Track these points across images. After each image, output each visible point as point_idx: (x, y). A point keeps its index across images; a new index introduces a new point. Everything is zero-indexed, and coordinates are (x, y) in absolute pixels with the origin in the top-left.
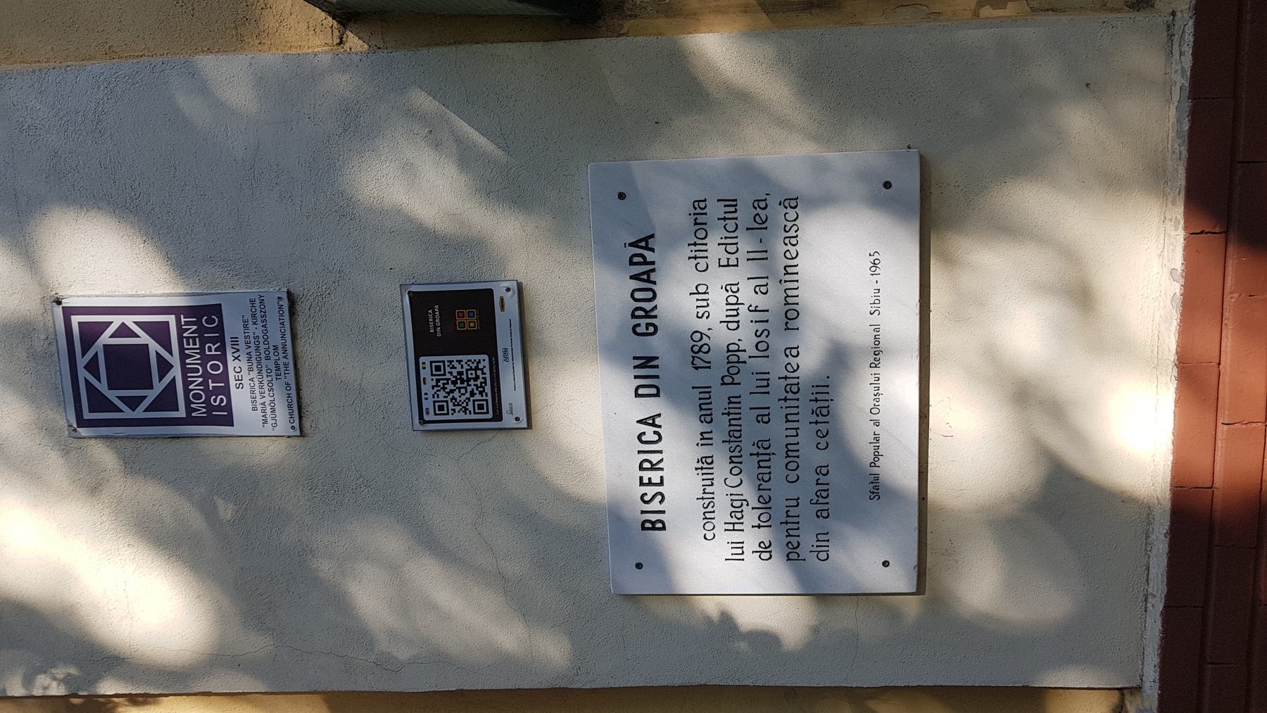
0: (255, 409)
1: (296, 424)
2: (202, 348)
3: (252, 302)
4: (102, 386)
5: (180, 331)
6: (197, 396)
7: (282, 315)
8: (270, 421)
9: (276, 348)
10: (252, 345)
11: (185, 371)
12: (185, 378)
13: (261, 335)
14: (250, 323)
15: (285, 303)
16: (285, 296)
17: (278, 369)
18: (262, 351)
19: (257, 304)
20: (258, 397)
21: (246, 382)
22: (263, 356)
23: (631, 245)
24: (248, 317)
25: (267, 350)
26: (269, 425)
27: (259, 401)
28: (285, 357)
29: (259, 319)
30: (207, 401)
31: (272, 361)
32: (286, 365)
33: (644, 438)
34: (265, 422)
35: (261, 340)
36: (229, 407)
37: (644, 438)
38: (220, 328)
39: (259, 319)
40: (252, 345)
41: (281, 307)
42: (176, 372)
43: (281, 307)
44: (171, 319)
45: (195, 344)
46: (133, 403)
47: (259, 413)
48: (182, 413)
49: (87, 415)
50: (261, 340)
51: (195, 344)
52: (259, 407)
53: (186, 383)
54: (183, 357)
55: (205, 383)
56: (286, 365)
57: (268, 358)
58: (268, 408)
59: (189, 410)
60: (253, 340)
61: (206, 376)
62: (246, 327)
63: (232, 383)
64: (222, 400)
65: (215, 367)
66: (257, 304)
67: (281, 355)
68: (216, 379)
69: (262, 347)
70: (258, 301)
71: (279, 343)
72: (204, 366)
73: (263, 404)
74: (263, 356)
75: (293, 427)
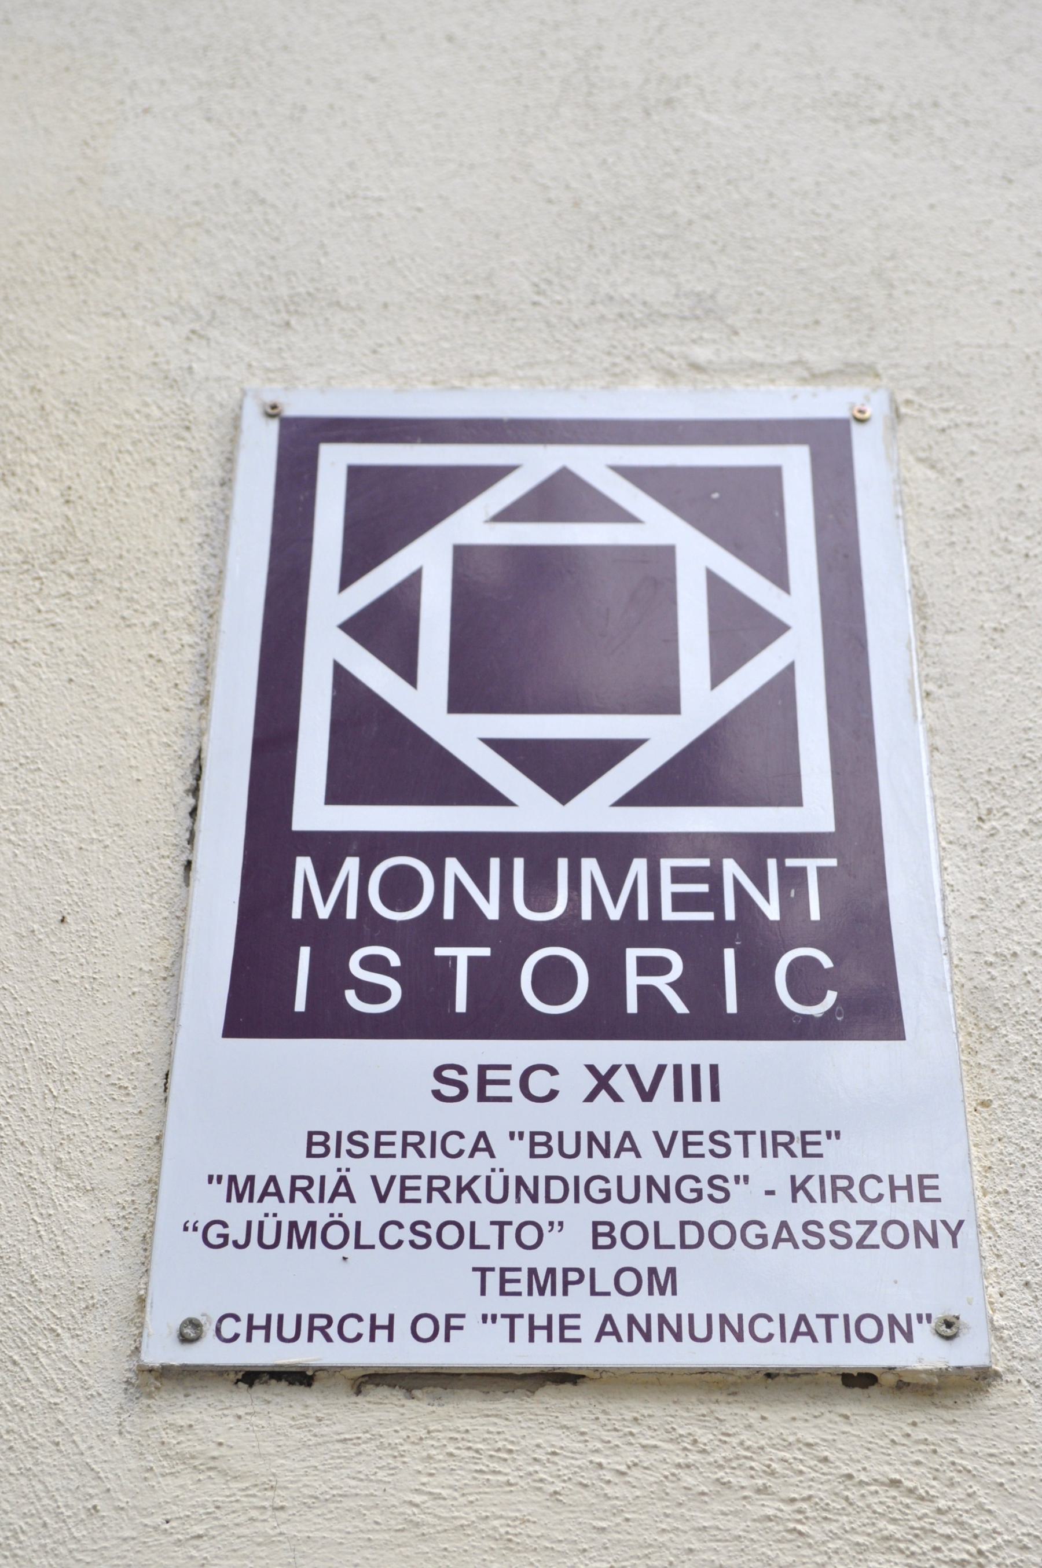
0: (316, 1143)
1: (208, 1352)
2: (656, 931)
3: (922, 1187)
4: (473, 524)
5: (754, 850)
6: (401, 888)
7: (853, 1329)
8: (238, 1215)
9: (664, 1282)
10: (676, 1166)
11: (542, 851)
12: (507, 845)
13: (736, 1211)
14: (802, 1167)
15: (924, 1354)
16: (967, 1353)
17: (542, 1282)
18: (647, 1211)
19: (908, 1211)
20: (384, 1170)
21: (470, 1116)
22: (616, 1213)
23: (343, 1179)
24: (835, 1159)
25: (651, 1236)
26: (213, 1203)
27: (361, 1172)
28: (607, 1328)
29: (826, 1213)
30: (371, 929)
31: (585, 1257)
32: (562, 1328)
33: (241, 1242)
34: (239, 1189)
35: (706, 1213)
36: (329, 1020)
37: (241, 1242)
38: (762, 1021)
39: (826, 1213)
40: (676, 1166)
41: (900, 1328)
42: (531, 809)
43: (900, 1328)
44: (816, 812)
45: (681, 902)
46: (387, 628)
47: (289, 1162)
48: (312, 810)
49: (334, 462)
50: (706, 1213)
51: (681, 902)
52: (327, 1168)
53: (475, 850)
54: (615, 851)
55: (468, 925)
56: (562, 1328)
57: (664, 1282)
58: (320, 1213)
59: (328, 850)
60: (706, 1167)
61: (512, 937)
62: (778, 1142)
63: (471, 1053)
64: (375, 994)
65: (554, 980)
66: (908, 1211)
67: (620, 1308)
68: (494, 982)
69: (669, 1215)
70: (926, 1214)
71: (688, 1301)
72: (564, 931)
73: (344, 1189)
74: (616, 1213)
75: (190, 1332)
